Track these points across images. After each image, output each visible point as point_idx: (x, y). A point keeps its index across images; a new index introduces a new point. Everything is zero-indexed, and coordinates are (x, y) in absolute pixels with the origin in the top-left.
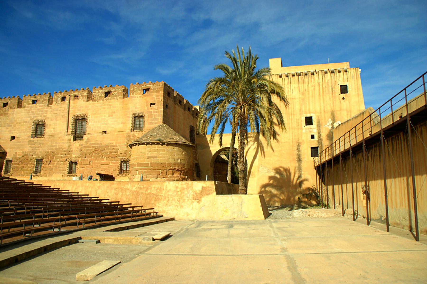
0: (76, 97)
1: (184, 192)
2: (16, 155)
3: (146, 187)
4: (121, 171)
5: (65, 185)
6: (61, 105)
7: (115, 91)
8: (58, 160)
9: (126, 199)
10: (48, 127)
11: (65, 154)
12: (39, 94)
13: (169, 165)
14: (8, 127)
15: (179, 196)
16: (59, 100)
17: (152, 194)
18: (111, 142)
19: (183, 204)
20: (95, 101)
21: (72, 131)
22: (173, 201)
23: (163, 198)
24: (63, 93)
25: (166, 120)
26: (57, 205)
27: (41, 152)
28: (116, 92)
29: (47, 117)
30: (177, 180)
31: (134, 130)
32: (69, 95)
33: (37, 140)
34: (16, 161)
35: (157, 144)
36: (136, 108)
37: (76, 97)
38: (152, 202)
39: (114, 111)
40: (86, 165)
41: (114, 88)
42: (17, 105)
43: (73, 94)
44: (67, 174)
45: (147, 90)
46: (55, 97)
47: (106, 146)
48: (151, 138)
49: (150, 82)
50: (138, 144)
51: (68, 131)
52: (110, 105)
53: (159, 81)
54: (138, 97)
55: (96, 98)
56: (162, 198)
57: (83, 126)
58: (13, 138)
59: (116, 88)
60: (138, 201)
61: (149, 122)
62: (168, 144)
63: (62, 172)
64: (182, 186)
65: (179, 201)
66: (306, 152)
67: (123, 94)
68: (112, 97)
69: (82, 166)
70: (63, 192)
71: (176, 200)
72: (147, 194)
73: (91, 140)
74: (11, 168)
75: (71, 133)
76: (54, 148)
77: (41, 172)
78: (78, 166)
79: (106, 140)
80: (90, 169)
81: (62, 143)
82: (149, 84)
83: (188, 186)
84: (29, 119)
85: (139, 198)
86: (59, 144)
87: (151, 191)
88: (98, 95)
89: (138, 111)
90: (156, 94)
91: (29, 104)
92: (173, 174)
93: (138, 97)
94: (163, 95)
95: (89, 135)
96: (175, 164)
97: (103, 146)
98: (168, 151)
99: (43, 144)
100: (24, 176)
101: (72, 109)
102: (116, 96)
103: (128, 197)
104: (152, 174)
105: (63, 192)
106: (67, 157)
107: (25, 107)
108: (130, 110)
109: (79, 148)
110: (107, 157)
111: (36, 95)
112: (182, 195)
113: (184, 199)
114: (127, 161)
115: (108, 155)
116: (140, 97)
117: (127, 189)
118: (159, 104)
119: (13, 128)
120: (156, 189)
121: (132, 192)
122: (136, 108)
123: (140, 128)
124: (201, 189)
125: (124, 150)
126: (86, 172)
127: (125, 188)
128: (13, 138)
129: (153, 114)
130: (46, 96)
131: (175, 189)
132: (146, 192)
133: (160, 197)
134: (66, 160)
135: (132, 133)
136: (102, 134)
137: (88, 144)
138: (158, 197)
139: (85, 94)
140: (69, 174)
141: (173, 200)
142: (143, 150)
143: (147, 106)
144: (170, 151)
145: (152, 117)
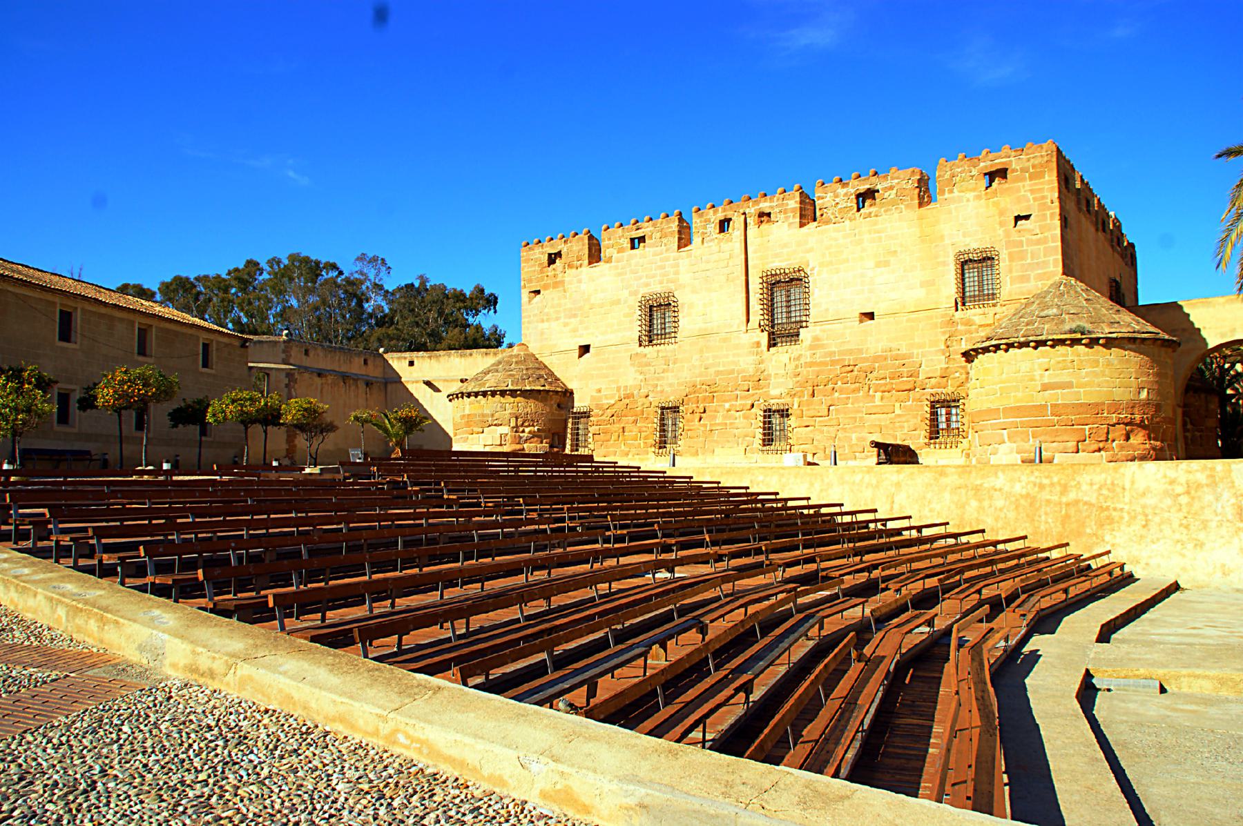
0: (764, 216)
1: (1199, 498)
2: (600, 398)
3: (1059, 483)
4: (934, 433)
5: (784, 480)
6: (719, 243)
7: (891, 188)
8: (727, 405)
9: (997, 520)
10: (685, 310)
11: (746, 388)
12: (647, 218)
13: (1115, 407)
14: (567, 320)
15: (1185, 509)
16: (712, 230)
17: (1086, 503)
18: (894, 345)
19: (1202, 536)
20: (828, 222)
21: (762, 317)
22: (1163, 527)
23: (1125, 515)
24: (720, 209)
25: (1067, 271)
27: (671, 385)
28: (895, 191)
30: (1143, 458)
31: (963, 304)
32: (742, 211)
33: (658, 351)
34: (601, 413)
35: (1071, 346)
36: (964, 235)
37: (765, 218)
38: (1088, 531)
39: (893, 249)
40: (818, 419)
41: (885, 177)
42: (587, 256)
43: (752, 210)
44: (760, 447)
45: (1000, 173)
46: (696, 222)
47: (876, 359)
48: (1046, 327)
49: (1006, 149)
50: (1032, 344)
51: (748, 321)
52: (878, 232)
53: (1038, 141)
54: (968, 200)
55: (829, 213)
56: (1122, 518)
57: (793, 303)
58: (585, 349)
59: (892, 179)
60: (1039, 528)
61: (1015, 274)
62: (1110, 343)
63: (743, 440)
64: (1191, 477)
65: (1187, 527)
67: (916, 196)
68: (882, 205)
69: (806, 421)
70: (705, 485)
71: (1176, 524)
72: (1068, 505)
73: (825, 342)
74: (590, 435)
75: (760, 326)
76: (712, 370)
77: (679, 442)
78: (792, 421)
79: (875, 339)
80: (831, 428)
81: (734, 355)
82: (1002, 153)
83: (1213, 476)
84: (625, 293)
85: (1040, 516)
86: (725, 360)
87: (1080, 494)
88: (834, 203)
89: (974, 243)
90: (1031, 185)
91: (621, 250)
92: (1128, 438)
93: (971, 199)
94: (1056, 185)
95: (818, 328)
96: (1132, 406)
97: (865, 360)
98: (1109, 364)
99: (675, 363)
100: (630, 456)
101: (755, 252)
102: (893, 203)
103: (1002, 515)
104: (1057, 439)
105: (705, 485)
106: (753, 395)
107: (609, 260)
108: (947, 241)
109: (791, 367)
110: (884, 392)
111: (637, 222)
112: (1196, 506)
113: (1207, 521)
114: (954, 401)
115: (885, 385)
116: (978, 197)
117: (996, 490)
118: (1044, 215)
119: (581, 322)
120: (1095, 487)
121: (1013, 499)
122: (964, 235)
123: (987, 296)
125: (938, 367)
126: (818, 438)
127: (986, 485)
128: (585, 349)
129: (1025, 248)
130: (668, 222)
131: (1167, 486)
132: (1064, 500)
133: (1114, 514)
134: (753, 406)
135: (959, 314)
136: (861, 321)
137: (818, 355)
138: (1106, 513)
139: (793, 203)
140: (764, 445)
141: (1162, 523)
142: (1024, 367)
143: (1002, 224)
144: (1116, 362)
145: (1023, 258)
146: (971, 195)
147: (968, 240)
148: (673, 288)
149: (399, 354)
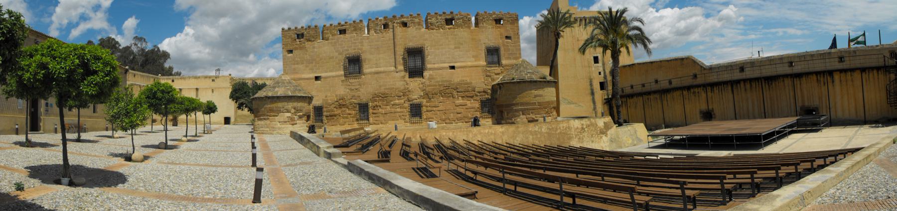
18: (464, 79)
26: (603, 180)
29: (364, 50)
54: (489, 28)
66: (597, 86)
71: (586, 136)
79: (457, 77)
89: (492, 44)
124: (603, 125)
133: (571, 135)
146: (490, 27)
147: (489, 42)
148: (361, 52)
149: (167, 77)
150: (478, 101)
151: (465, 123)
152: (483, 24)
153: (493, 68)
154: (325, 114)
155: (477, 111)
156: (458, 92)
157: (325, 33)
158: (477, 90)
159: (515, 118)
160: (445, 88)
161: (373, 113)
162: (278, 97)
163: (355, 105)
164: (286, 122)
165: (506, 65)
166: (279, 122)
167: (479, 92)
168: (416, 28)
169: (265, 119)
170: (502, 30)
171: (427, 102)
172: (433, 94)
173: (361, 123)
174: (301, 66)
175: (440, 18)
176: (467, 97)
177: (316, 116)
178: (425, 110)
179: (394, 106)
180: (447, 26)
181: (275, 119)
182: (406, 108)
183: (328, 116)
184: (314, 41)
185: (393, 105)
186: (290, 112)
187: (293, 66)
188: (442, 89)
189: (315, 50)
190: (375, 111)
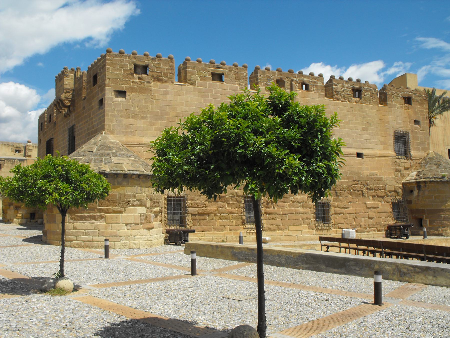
18: (374, 172)
146: (399, 106)
150: (389, 203)
151: (377, 232)
152: (392, 102)
153: (402, 161)
154: (190, 210)
155: (389, 216)
156: (368, 189)
157: (189, 72)
158: (388, 188)
159: (444, 229)
160: (355, 182)
161: (266, 213)
162: (125, 176)
163: (239, 199)
164: (138, 224)
165: (416, 158)
166: (127, 224)
167: (390, 191)
168: (320, 94)
169: (94, 218)
170: (411, 112)
171: (335, 200)
172: (341, 190)
173: (248, 228)
174: (140, 122)
175: (347, 86)
176: (378, 196)
177: (168, 214)
178: (334, 212)
179: (295, 204)
180: (354, 99)
181: (117, 218)
182: (310, 208)
183: (195, 215)
184: (166, 82)
185: (294, 202)
186: (145, 206)
187: (125, 121)
188: (351, 183)
189: (169, 97)
190: (268, 210)
